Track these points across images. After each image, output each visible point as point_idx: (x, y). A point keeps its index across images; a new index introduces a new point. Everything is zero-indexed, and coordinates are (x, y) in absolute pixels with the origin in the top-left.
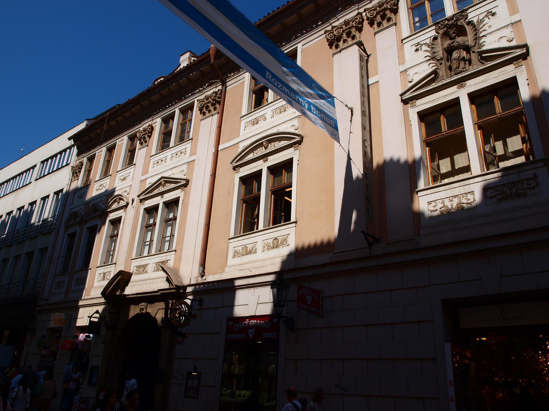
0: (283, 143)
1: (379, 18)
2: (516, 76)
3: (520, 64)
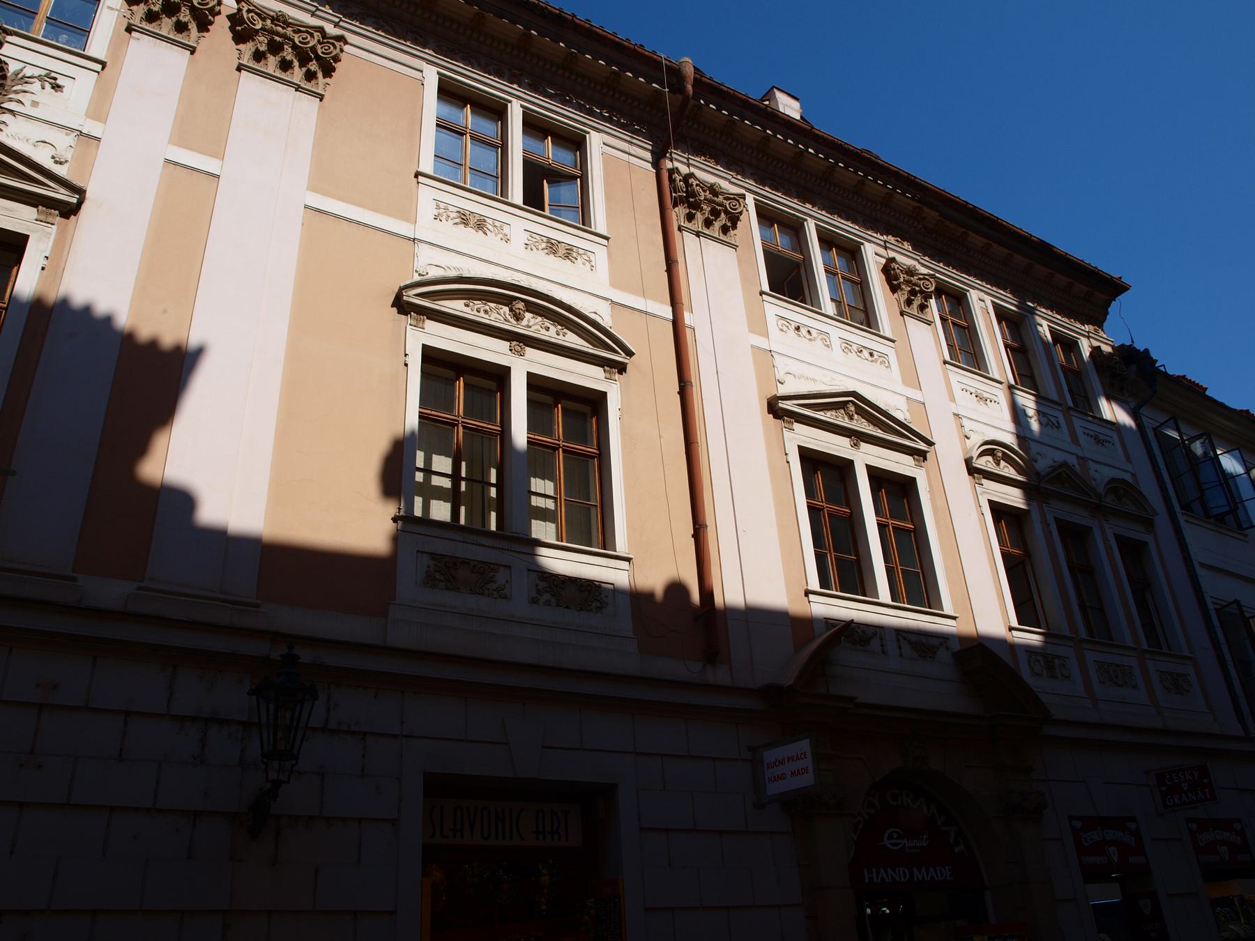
0: (572, 340)
1: (262, 43)
2: (25, 238)
3: (50, 220)
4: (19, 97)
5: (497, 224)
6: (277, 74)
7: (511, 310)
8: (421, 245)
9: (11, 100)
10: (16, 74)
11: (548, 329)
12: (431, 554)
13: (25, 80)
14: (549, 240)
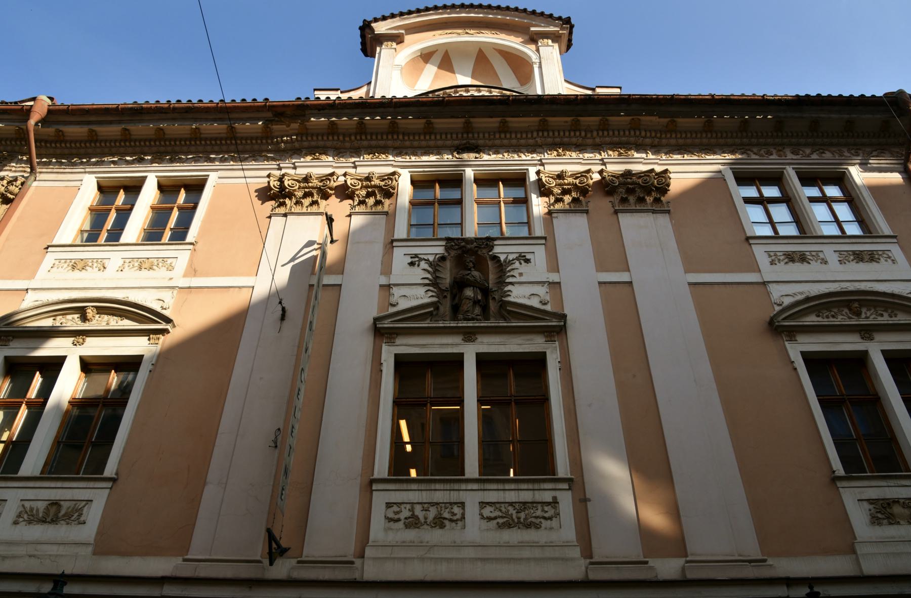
2: (463, 354)
4: (512, 273)
5: (814, 253)
6: (638, 208)
7: (850, 310)
8: (770, 285)
9: (509, 277)
10: (505, 261)
11: (882, 315)
12: (868, 500)
13: (511, 263)
14: (854, 253)
